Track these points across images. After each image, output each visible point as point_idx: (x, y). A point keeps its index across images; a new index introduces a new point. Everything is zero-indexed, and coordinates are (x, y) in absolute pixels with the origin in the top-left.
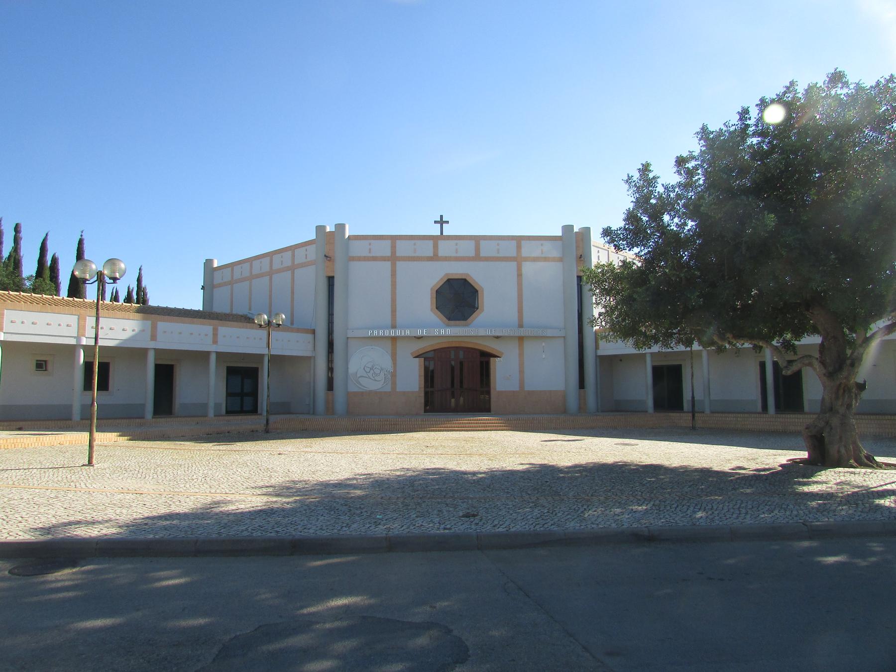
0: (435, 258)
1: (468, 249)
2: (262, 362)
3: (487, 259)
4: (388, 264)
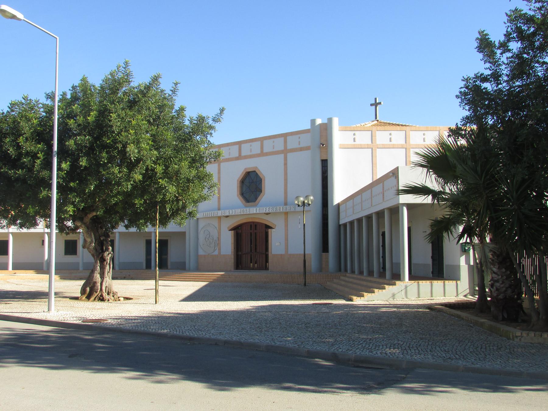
0: (240, 157)
1: (256, 148)
2: (8, 237)
3: (246, 157)
4: (290, 155)
